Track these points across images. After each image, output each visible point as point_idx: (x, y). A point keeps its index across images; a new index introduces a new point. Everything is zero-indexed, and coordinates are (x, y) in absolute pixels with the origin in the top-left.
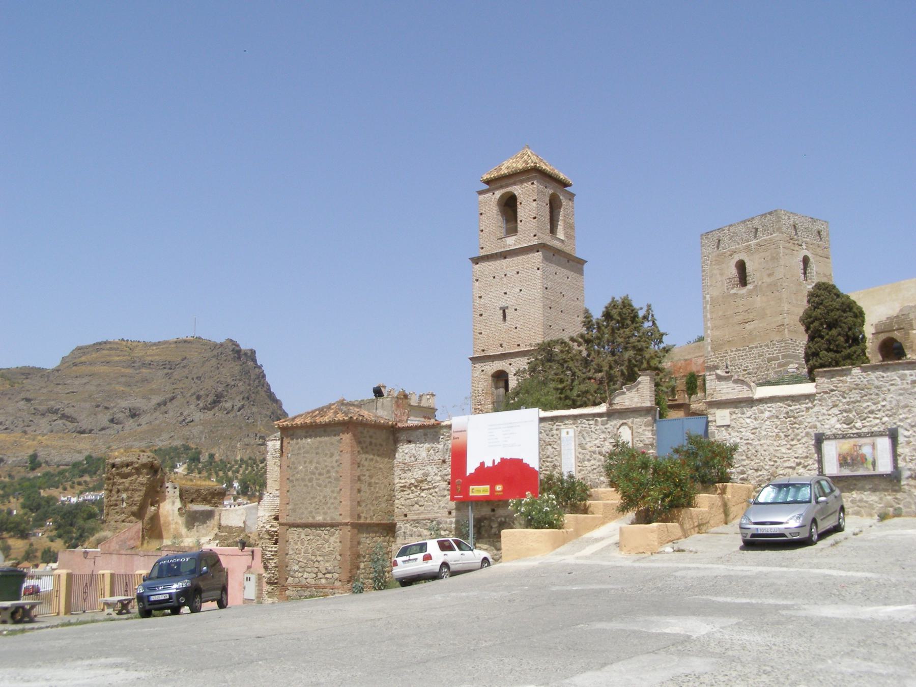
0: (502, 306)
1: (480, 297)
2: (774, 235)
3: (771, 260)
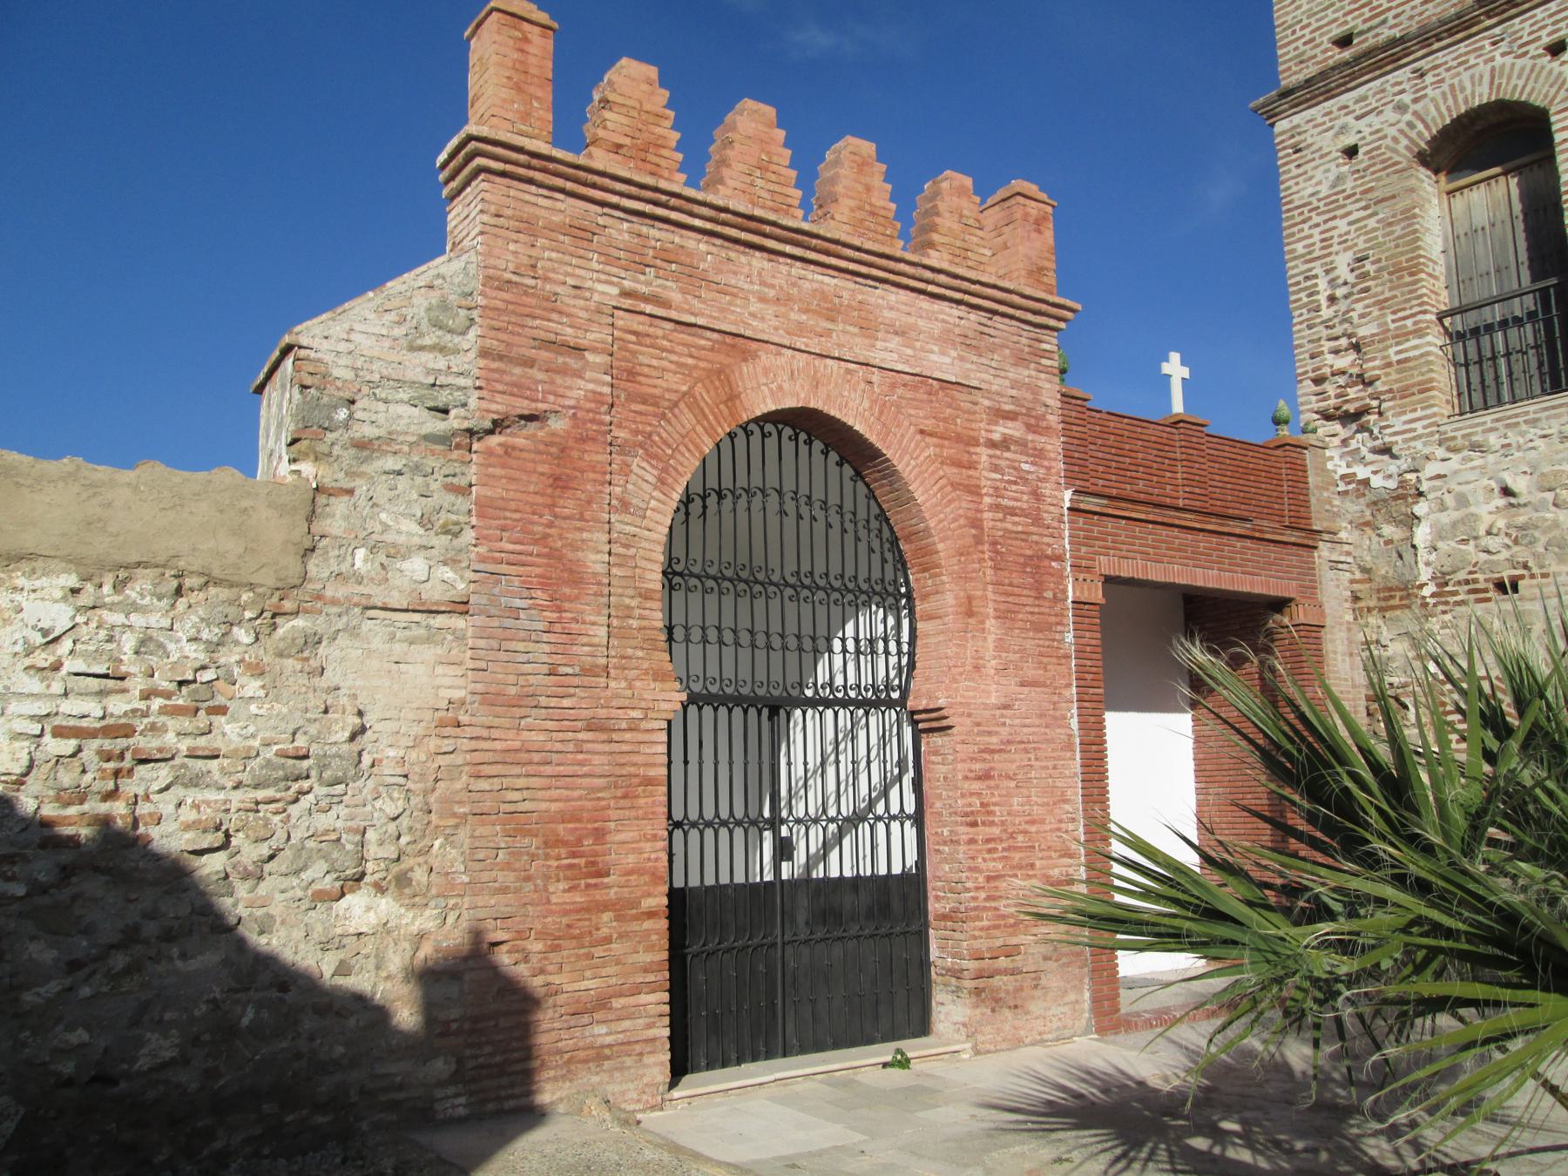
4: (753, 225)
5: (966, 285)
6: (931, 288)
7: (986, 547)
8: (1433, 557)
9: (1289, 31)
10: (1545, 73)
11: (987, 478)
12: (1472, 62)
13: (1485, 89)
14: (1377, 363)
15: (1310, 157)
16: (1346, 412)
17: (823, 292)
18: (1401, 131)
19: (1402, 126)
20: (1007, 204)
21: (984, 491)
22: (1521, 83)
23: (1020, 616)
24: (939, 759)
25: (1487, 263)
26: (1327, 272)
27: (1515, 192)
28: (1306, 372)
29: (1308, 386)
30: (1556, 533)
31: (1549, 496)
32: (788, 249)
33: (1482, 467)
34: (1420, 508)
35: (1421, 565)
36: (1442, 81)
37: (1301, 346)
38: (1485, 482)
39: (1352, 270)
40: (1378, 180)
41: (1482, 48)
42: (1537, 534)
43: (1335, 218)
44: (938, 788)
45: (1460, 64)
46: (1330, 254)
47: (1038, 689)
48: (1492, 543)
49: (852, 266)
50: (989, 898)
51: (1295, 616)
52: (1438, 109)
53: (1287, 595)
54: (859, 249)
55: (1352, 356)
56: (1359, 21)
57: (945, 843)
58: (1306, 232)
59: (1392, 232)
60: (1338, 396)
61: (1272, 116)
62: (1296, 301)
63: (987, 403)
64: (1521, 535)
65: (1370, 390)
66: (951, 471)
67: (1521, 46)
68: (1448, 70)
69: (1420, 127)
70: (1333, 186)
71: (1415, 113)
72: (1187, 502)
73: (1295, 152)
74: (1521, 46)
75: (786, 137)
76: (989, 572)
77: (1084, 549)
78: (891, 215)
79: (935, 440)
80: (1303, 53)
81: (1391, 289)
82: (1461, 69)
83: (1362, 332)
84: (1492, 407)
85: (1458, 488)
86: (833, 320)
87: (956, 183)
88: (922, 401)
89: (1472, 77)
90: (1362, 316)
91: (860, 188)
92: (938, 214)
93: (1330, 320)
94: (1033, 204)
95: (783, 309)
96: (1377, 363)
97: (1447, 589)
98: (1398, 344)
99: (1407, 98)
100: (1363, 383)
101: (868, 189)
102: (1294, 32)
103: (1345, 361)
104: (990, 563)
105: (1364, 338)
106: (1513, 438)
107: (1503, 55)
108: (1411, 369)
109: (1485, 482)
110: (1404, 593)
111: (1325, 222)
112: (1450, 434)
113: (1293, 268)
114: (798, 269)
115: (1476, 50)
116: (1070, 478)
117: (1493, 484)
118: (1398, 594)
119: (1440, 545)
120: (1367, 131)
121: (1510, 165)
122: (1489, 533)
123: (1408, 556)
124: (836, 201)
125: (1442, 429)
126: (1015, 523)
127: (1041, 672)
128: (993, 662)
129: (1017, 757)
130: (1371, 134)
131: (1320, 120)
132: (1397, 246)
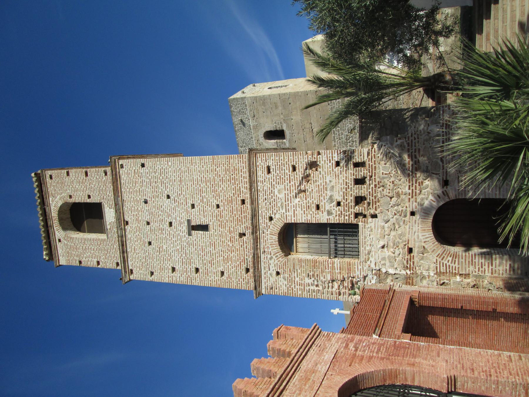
0: (186, 231)
1: (174, 269)
2: (247, 103)
3: (265, 106)
4: (275, 390)
5: (304, 346)
6: (303, 354)
7: (390, 357)
8: (399, 269)
9: (238, 285)
10: (276, 222)
11: (367, 353)
12: (266, 239)
13: (274, 237)
14: (339, 276)
15: (275, 285)
16: (351, 287)
17: (300, 380)
18: (277, 259)
19: (276, 259)
20: (279, 336)
21: (371, 355)
22: (276, 228)
23: (415, 353)
24: (466, 384)
25: (318, 246)
26: (309, 286)
27: (302, 236)
28: (336, 297)
29: (341, 297)
30: (397, 236)
31: (386, 236)
32: (284, 384)
33: (375, 252)
34: (384, 270)
35: (400, 273)
36: (268, 247)
37: (328, 298)
38: (379, 252)
39: (311, 278)
40: (288, 267)
41: (263, 236)
42: (396, 241)
43: (294, 281)
44: (476, 387)
45: (266, 242)
46: (304, 284)
47: (440, 353)
48: (397, 252)
49: (293, 370)
50: (518, 375)
51: (416, 297)
52: (274, 249)
53: (409, 297)
54: (288, 367)
55: (335, 283)
56: (244, 266)
57: (498, 387)
58: (296, 290)
59: (304, 266)
60: (346, 289)
61: (259, 294)
62: (315, 296)
63: (342, 349)
64: (396, 245)
65: (346, 279)
66: (364, 361)
67: (267, 227)
68: (266, 245)
69: (278, 254)
70: (285, 280)
71: (274, 255)
72: (378, 313)
73: (272, 289)
74: (267, 227)
75: (248, 377)
76: (399, 358)
77: (392, 336)
78: (278, 359)
79: (353, 363)
80: (246, 282)
81: (319, 269)
82: (267, 242)
83: (329, 278)
84: (359, 249)
85: (380, 259)
86: (309, 379)
87: (271, 343)
88: (340, 364)
89: (270, 239)
90: (324, 278)
91: (268, 364)
92: (280, 349)
93: (323, 287)
94: (281, 329)
95: (304, 390)
96: (339, 276)
97: (409, 267)
98: (335, 269)
99: (269, 256)
100: (343, 281)
101: (269, 362)
102: (239, 284)
103: (336, 285)
104: (396, 357)
105: (331, 278)
106: (369, 243)
107: (267, 231)
108: (343, 267)
109: (379, 252)
110: (408, 279)
111: (295, 284)
112: (364, 259)
113: (305, 295)
114: (291, 384)
115: (263, 238)
116: (369, 335)
117: (380, 250)
118: (408, 280)
119: (395, 267)
120: (274, 268)
121: (294, 236)
122: (394, 253)
123: (397, 276)
124: (271, 370)
125: (362, 261)
126: (383, 349)
127: (434, 352)
128: (431, 362)
129: (465, 362)
130: (275, 267)
131: (266, 280)
132: (308, 265)
